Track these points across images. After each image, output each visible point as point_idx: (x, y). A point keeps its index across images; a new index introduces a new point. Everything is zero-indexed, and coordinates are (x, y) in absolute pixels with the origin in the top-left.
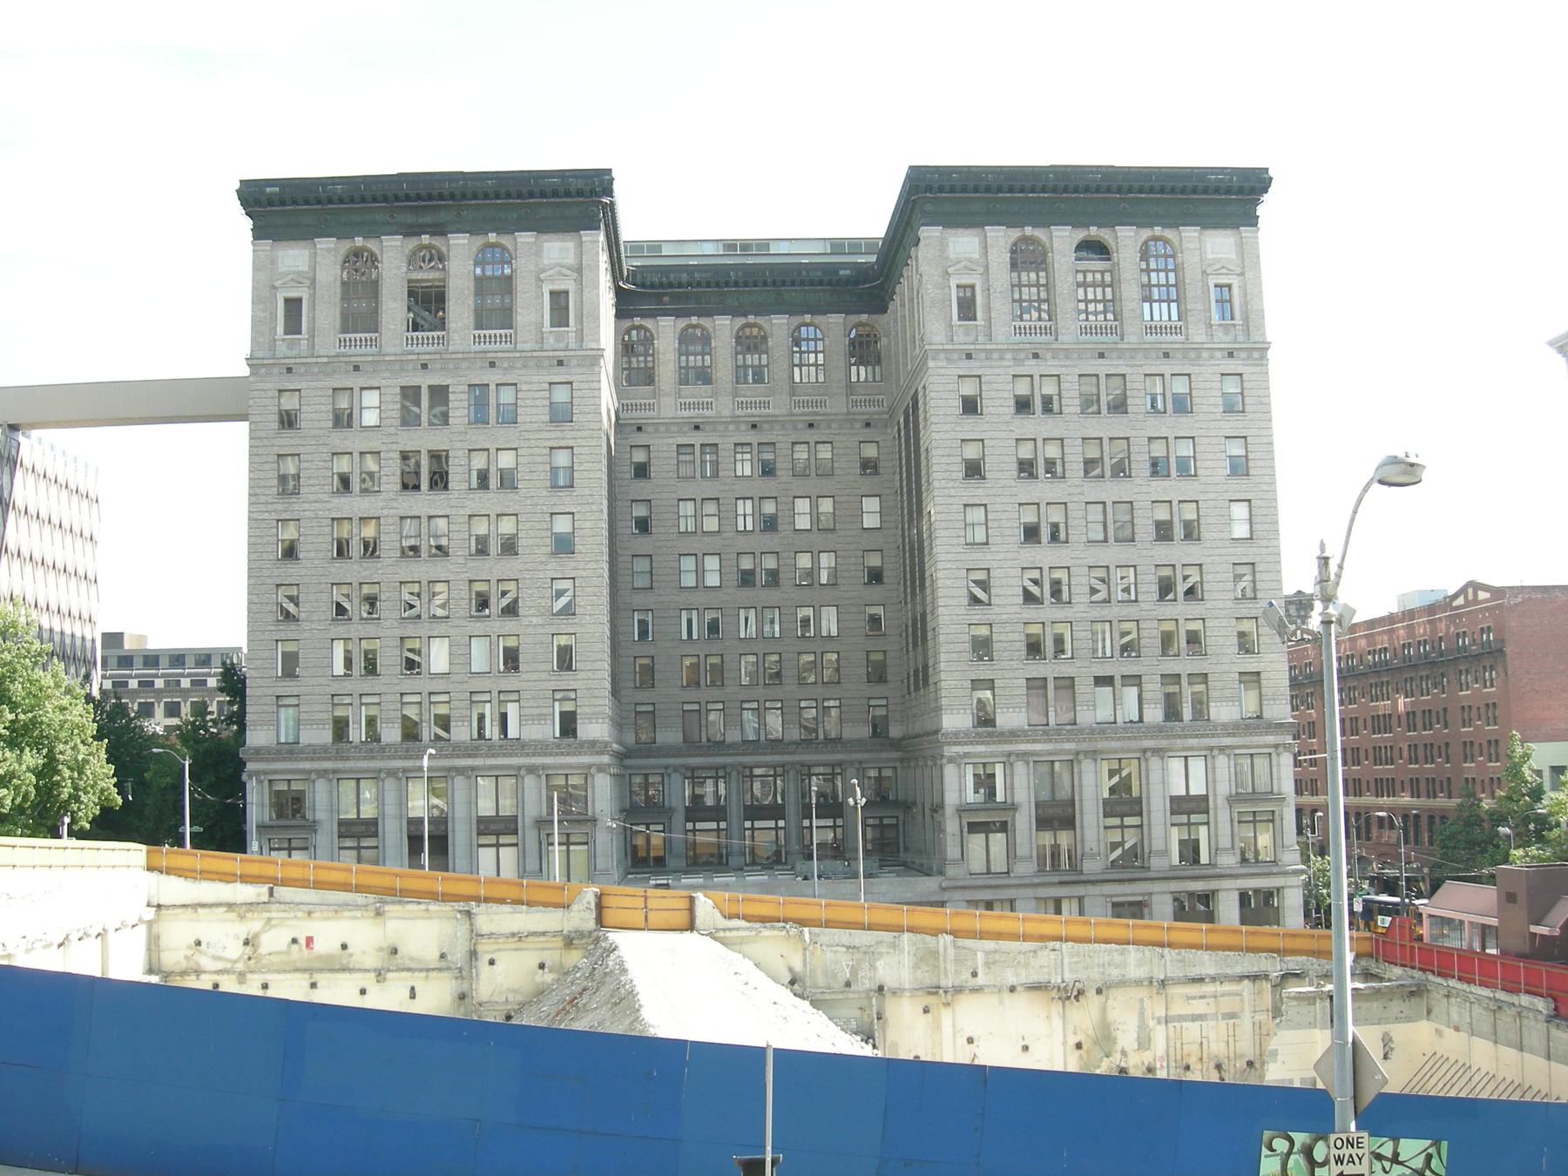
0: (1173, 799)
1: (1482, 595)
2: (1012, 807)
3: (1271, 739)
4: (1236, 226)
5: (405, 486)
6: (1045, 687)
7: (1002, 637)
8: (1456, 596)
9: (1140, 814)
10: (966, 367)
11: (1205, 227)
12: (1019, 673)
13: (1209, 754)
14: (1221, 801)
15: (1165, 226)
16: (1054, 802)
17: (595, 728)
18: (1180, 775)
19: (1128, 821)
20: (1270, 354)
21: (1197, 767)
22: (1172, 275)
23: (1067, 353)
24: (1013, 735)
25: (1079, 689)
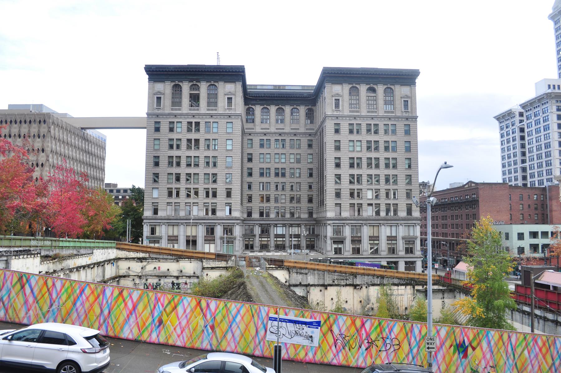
0: (387, 237)
1: (473, 185)
2: (160, 238)
3: (414, 222)
6: (354, 206)
11: (225, 82)
14: (400, 238)
15: (391, 85)
24: (346, 219)
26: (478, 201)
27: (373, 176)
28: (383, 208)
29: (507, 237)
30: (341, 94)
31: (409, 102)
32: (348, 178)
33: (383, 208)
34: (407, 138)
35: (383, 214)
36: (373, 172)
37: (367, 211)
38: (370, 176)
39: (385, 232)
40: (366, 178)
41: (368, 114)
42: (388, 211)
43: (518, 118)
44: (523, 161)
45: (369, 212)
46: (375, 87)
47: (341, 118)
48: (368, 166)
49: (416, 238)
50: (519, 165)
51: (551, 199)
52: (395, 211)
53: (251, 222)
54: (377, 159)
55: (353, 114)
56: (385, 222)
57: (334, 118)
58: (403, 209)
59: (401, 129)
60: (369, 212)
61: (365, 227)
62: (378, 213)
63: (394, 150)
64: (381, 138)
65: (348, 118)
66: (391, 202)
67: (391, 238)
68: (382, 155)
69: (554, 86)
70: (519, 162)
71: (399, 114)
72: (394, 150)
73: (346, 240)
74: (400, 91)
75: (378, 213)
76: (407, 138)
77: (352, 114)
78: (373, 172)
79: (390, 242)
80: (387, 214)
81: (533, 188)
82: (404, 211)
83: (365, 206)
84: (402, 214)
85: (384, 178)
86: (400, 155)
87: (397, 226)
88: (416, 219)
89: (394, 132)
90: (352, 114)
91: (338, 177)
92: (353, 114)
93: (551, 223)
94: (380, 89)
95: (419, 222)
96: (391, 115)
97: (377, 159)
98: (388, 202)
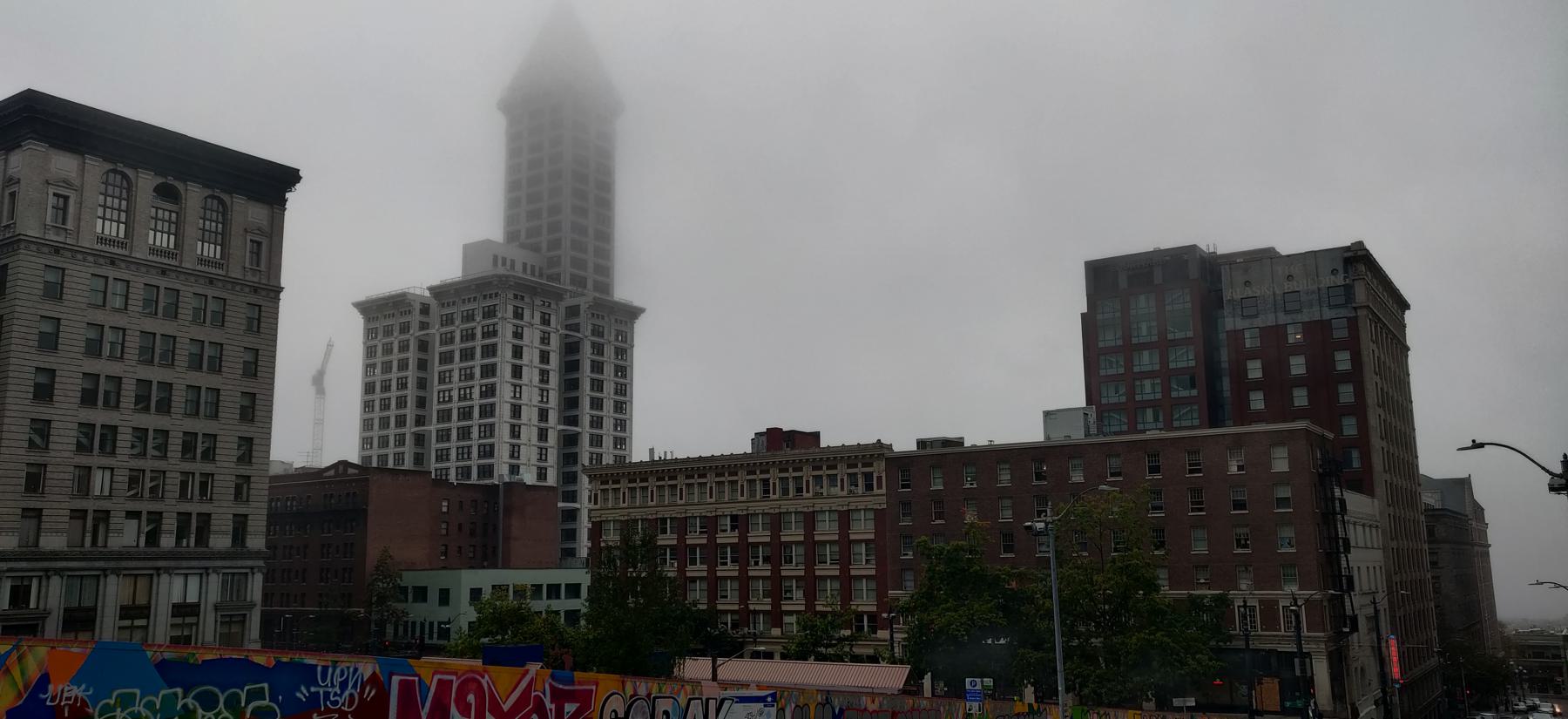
0: (174, 606)
1: (351, 471)
2: (44, 615)
3: (250, 563)
4: (82, 154)
5: (244, 374)
6: (84, 518)
7: (55, 476)
8: (328, 469)
9: (148, 617)
10: (253, 299)
11: (250, 198)
12: (63, 505)
13: (204, 573)
14: (210, 607)
15: (223, 191)
16: (80, 609)
17: (256, 542)
18: (173, 589)
19: (138, 622)
20: (282, 295)
21: (193, 583)
22: (124, 203)
23: (138, 264)
24: (55, 556)
25: (113, 520)
26: (365, 511)
27: (151, 433)
28: (170, 523)
29: (445, 597)
30: (77, 182)
31: (71, 201)
32: (74, 433)
33: (170, 523)
34: (250, 341)
35: (167, 542)
36: (151, 421)
37: (120, 532)
38: (141, 434)
39: (173, 589)
40: (129, 437)
41: (199, 268)
42: (181, 533)
43: (416, 318)
44: (420, 421)
45: (127, 535)
46: (179, 186)
47: (69, 254)
48: (136, 404)
49: (252, 605)
50: (410, 429)
51: (508, 511)
52: (202, 538)
53: (240, 563)
54: (167, 387)
55: (107, 248)
56: (172, 564)
57: (45, 250)
58: (61, 526)
59: (237, 315)
60: (127, 535)
61: (112, 579)
62: (153, 538)
63: (216, 367)
64: (185, 331)
65: (90, 258)
66: (194, 508)
67: (184, 610)
68: (181, 377)
69: (504, 260)
70: (410, 420)
71: (236, 273)
72: (216, 367)
73: (48, 621)
74: (250, 213)
75: (153, 538)
76: (250, 341)
77: (103, 247)
78: (151, 421)
79: (179, 620)
80: (179, 538)
81: (441, 482)
82: (225, 533)
83: (117, 519)
84: (220, 541)
85: (180, 441)
86: (230, 384)
87: (204, 573)
88: (257, 555)
89: (220, 320)
90: (103, 247)
91: (42, 429)
92: (107, 248)
93: (506, 565)
94: (194, 195)
95: (261, 563)
96: (214, 270)
97: (167, 387)
98: (185, 507)
